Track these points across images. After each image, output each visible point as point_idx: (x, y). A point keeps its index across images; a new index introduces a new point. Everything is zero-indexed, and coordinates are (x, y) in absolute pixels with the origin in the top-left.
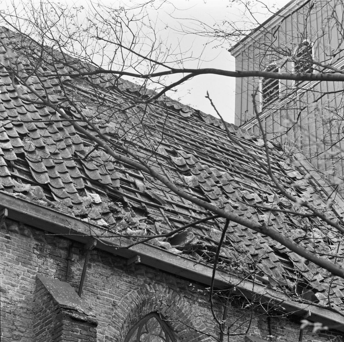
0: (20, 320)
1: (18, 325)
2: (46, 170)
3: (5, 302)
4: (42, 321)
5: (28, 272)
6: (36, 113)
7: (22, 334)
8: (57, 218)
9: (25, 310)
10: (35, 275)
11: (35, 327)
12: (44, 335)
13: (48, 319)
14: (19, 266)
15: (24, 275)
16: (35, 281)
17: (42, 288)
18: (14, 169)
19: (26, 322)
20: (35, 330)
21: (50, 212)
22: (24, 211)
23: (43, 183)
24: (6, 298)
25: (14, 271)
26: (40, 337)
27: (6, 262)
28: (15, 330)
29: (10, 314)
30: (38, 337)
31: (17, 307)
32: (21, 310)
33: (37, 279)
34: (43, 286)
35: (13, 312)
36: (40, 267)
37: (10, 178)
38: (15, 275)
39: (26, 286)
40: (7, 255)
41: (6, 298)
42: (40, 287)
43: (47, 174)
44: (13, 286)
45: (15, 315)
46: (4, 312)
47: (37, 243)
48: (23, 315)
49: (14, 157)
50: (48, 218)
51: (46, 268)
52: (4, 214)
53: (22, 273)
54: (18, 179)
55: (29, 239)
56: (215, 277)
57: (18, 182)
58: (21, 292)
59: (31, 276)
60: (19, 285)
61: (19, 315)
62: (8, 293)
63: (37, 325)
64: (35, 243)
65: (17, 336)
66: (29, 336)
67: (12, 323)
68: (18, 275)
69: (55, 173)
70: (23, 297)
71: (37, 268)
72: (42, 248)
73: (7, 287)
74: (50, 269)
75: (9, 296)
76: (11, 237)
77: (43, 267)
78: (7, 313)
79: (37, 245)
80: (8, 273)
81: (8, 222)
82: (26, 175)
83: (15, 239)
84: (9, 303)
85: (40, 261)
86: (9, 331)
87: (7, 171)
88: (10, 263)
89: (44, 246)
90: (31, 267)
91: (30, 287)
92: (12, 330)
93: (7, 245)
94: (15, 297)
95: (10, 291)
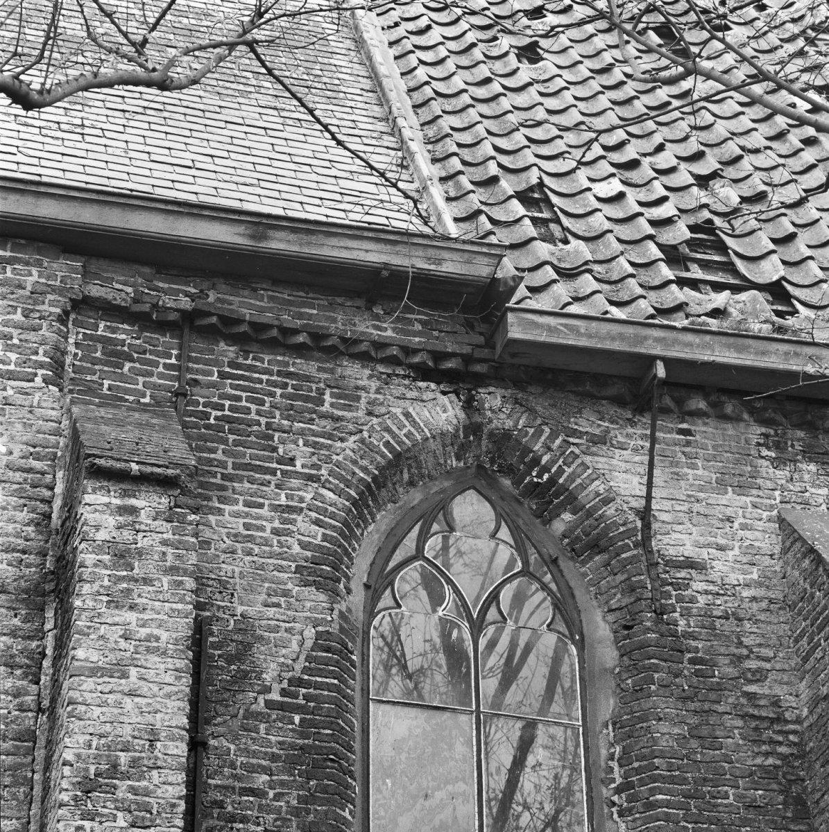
0: (756, 630)
1: (752, 643)
2: (772, 246)
3: (707, 592)
4: (808, 622)
5: (755, 506)
6: (742, 117)
7: (768, 666)
8: (796, 354)
9: (764, 605)
10: (775, 513)
11: (796, 641)
12: (819, 657)
13: (820, 614)
14: (727, 497)
15: (744, 517)
16: (777, 525)
17: (795, 541)
18: (689, 264)
19: (773, 633)
20: (799, 649)
21: (775, 346)
22: (706, 356)
23: (768, 281)
24: (707, 581)
25: (718, 512)
26: (812, 664)
27: (689, 493)
28: (748, 657)
29: (727, 619)
30: (808, 666)
31: (742, 600)
32: (754, 604)
33: (781, 520)
34: (796, 535)
35: (734, 614)
36: (783, 489)
37: (674, 287)
38: (722, 520)
39: (756, 544)
40: (690, 477)
41: (707, 581)
42: (791, 540)
43: (774, 257)
44: (721, 548)
45: (740, 620)
46: (710, 617)
47: (764, 430)
48: (762, 617)
49: (684, 234)
50: (775, 359)
51: (799, 489)
52: (655, 376)
53: (740, 512)
54: (702, 286)
55: (742, 425)
56: (827, 303)
57: (701, 293)
58: (745, 560)
59: (764, 516)
60: (737, 544)
61: (749, 619)
62: (712, 568)
63: (801, 636)
64: (759, 432)
65: (754, 672)
66: (786, 667)
67: (736, 641)
68: (729, 519)
69: (798, 250)
70: (752, 573)
71: (777, 493)
72: (778, 441)
73: (704, 554)
74: (813, 490)
75: (714, 576)
76: (693, 428)
77: (792, 488)
78: (719, 617)
79: (766, 436)
80: (701, 519)
81: (676, 394)
82: (724, 271)
83: (705, 431)
84: (718, 594)
85: (782, 474)
86: (732, 662)
87: (666, 272)
88: (702, 495)
89: (785, 434)
90: (761, 493)
91: (767, 540)
92: (740, 659)
93: (687, 450)
94: (732, 575)
95: (714, 563)
